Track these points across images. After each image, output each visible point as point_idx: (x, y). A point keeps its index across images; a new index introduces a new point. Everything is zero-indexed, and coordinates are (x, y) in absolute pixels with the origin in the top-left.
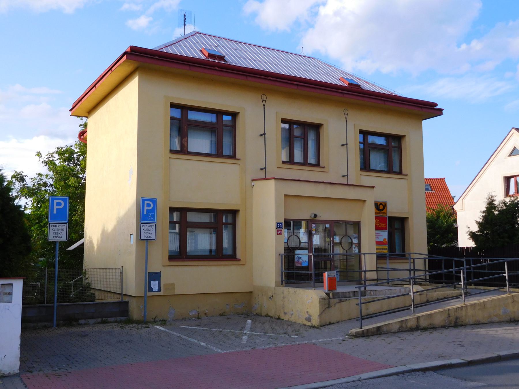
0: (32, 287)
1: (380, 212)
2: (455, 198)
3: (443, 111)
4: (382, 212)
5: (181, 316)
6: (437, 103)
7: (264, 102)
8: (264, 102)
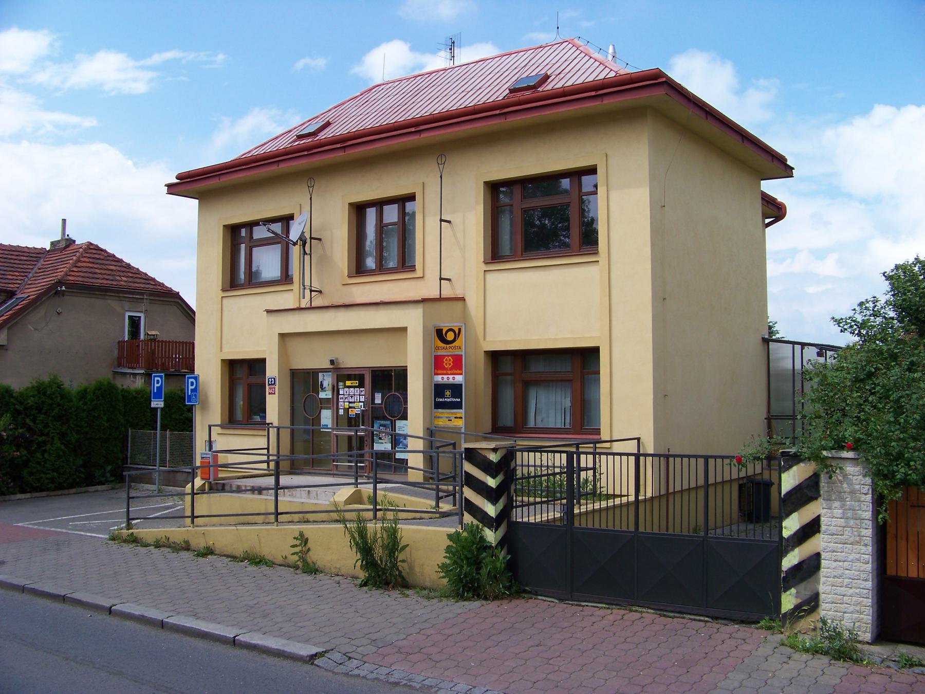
0: (510, 584)
1: (448, 346)
2: (838, 317)
3: (793, 170)
4: (451, 345)
5: (492, 612)
6: (786, 157)
7: (311, 189)
8: (311, 189)
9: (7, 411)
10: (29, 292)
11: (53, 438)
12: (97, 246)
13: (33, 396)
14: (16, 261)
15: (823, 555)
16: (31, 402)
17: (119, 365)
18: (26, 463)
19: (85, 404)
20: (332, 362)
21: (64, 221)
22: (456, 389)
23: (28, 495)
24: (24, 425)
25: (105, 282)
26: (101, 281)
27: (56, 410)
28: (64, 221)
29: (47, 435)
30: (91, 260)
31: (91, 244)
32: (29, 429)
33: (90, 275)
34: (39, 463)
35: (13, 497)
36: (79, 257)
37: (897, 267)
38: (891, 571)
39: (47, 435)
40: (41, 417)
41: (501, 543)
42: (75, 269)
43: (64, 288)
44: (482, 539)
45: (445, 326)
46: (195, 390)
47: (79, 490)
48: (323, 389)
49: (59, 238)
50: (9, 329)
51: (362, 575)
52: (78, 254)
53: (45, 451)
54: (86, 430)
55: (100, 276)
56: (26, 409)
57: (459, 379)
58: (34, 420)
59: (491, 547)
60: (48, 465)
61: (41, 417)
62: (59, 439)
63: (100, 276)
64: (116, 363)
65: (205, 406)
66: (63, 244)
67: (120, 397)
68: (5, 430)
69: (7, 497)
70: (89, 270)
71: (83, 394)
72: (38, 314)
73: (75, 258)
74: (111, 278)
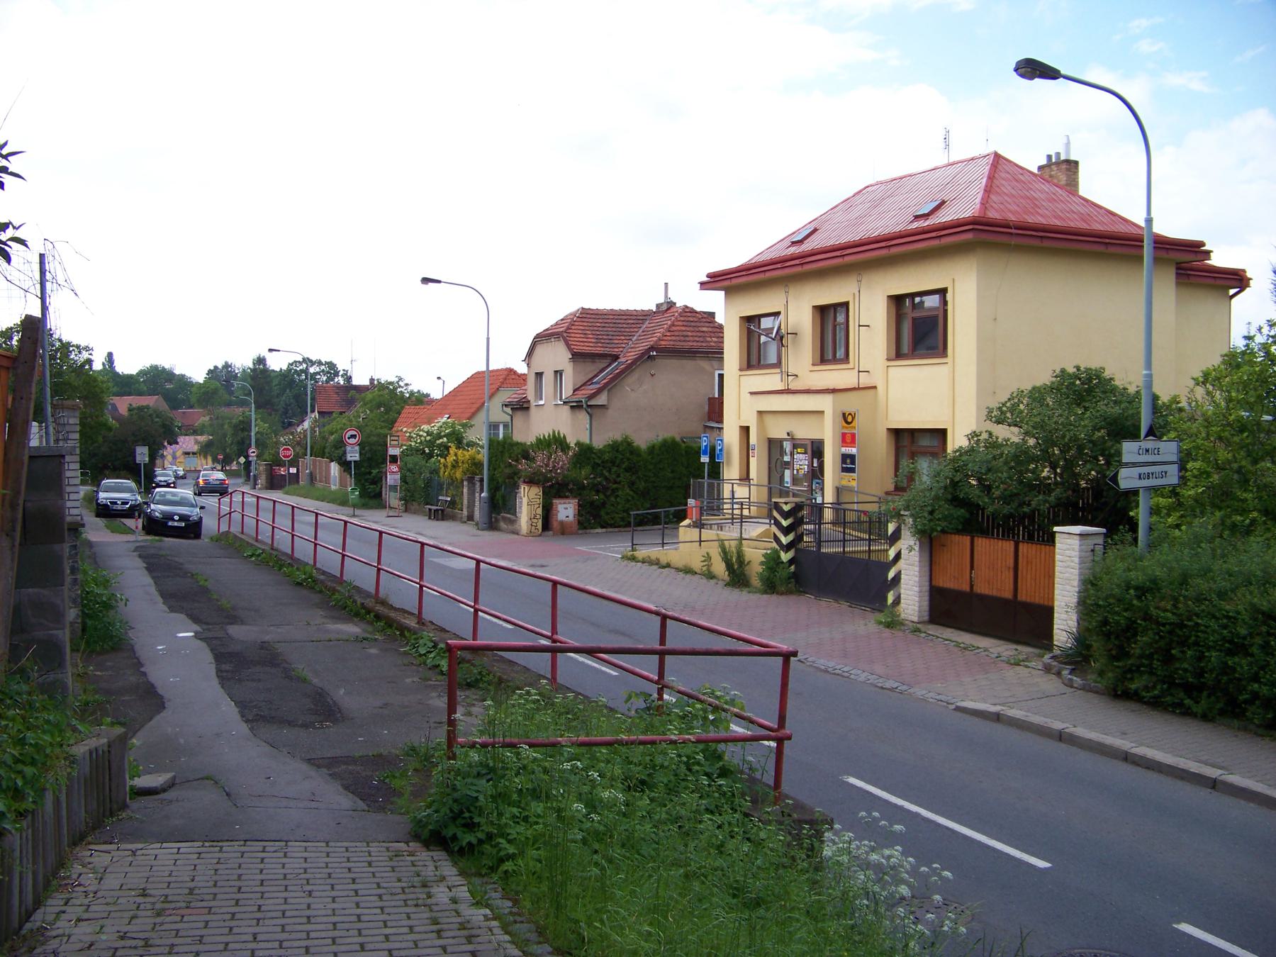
9: (589, 464)
10: (628, 356)
11: (624, 485)
12: (692, 309)
13: (609, 452)
14: (625, 326)
15: (902, 572)
16: (606, 457)
17: (710, 419)
18: (604, 504)
19: (652, 458)
20: (788, 434)
21: (666, 284)
22: (852, 457)
23: (604, 530)
24: (602, 475)
25: (695, 344)
26: (690, 344)
27: (626, 464)
28: (666, 284)
29: (619, 483)
30: (685, 323)
31: (687, 307)
32: (606, 479)
33: (682, 338)
34: (613, 505)
35: (592, 531)
36: (674, 321)
37: (1034, 388)
38: (934, 583)
39: (619, 483)
40: (614, 469)
41: (791, 562)
42: (668, 334)
43: (655, 353)
44: (779, 557)
45: (847, 411)
46: (721, 450)
47: (648, 528)
48: (786, 454)
49: (663, 301)
50: (609, 390)
51: (727, 578)
52: (673, 318)
53: (617, 496)
54: (653, 479)
55: (691, 338)
56: (603, 462)
57: (853, 451)
58: (610, 471)
59: (783, 562)
60: (619, 507)
61: (614, 469)
62: (629, 486)
63: (691, 338)
64: (707, 417)
65: (729, 463)
66: (665, 307)
67: (684, 452)
68: (586, 479)
69: (588, 531)
70: (681, 333)
71: (652, 449)
72: (632, 379)
73: (673, 318)
74: (701, 339)
